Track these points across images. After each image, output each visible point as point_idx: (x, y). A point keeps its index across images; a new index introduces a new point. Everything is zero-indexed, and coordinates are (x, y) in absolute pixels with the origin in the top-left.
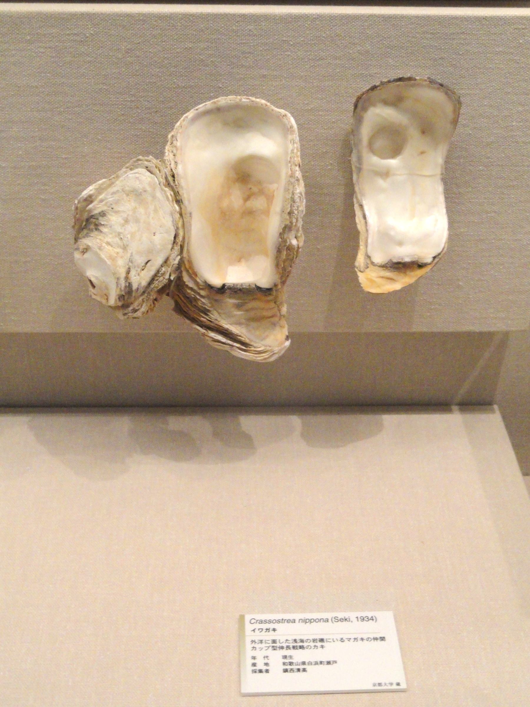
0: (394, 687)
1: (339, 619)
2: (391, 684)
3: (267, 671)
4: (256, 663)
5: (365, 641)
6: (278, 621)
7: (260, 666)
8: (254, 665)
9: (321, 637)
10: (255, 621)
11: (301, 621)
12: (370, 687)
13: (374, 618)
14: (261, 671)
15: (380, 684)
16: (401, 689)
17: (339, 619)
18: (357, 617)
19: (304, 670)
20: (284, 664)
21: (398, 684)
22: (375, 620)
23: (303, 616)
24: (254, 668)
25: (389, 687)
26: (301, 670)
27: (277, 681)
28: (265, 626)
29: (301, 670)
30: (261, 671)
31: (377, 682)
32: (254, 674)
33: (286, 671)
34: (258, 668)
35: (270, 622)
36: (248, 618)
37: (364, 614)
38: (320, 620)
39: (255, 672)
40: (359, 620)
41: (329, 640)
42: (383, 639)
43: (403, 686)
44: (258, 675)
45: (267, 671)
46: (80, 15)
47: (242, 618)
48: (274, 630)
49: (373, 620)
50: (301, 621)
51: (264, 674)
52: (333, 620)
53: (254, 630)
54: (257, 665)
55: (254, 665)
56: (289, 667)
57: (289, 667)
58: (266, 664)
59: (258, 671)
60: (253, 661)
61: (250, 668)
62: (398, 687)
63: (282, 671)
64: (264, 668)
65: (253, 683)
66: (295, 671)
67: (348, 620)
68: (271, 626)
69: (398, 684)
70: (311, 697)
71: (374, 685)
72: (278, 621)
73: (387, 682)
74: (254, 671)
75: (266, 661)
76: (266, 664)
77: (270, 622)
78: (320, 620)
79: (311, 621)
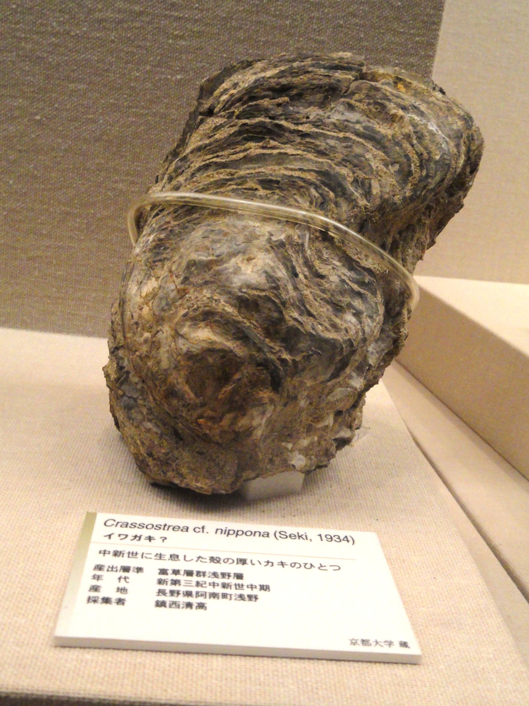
0: (397, 650)
1: (288, 535)
2: (390, 644)
3: (120, 601)
5: (288, 568)
10: (115, 523)
11: (219, 531)
13: (349, 539)
14: (107, 600)
15: (365, 642)
16: (407, 656)
17: (288, 535)
18: (320, 535)
19: (201, 606)
20: (160, 582)
22: (351, 542)
24: (93, 594)
25: (385, 650)
26: (195, 605)
28: (131, 532)
29: (195, 605)
30: (107, 600)
31: (359, 637)
33: (161, 604)
34: (101, 594)
36: (101, 517)
37: (332, 532)
38: (254, 534)
40: (324, 538)
41: (148, 556)
43: (414, 650)
46: (459, 199)
49: (348, 541)
50: (219, 531)
51: (113, 607)
52: (278, 535)
53: (110, 536)
56: (168, 599)
57: (168, 599)
59: (100, 600)
60: (95, 583)
61: (85, 593)
63: (154, 603)
64: (115, 596)
66: (181, 606)
67: (304, 537)
71: (354, 642)
72: (158, 527)
78: (254, 534)
79: (237, 533)
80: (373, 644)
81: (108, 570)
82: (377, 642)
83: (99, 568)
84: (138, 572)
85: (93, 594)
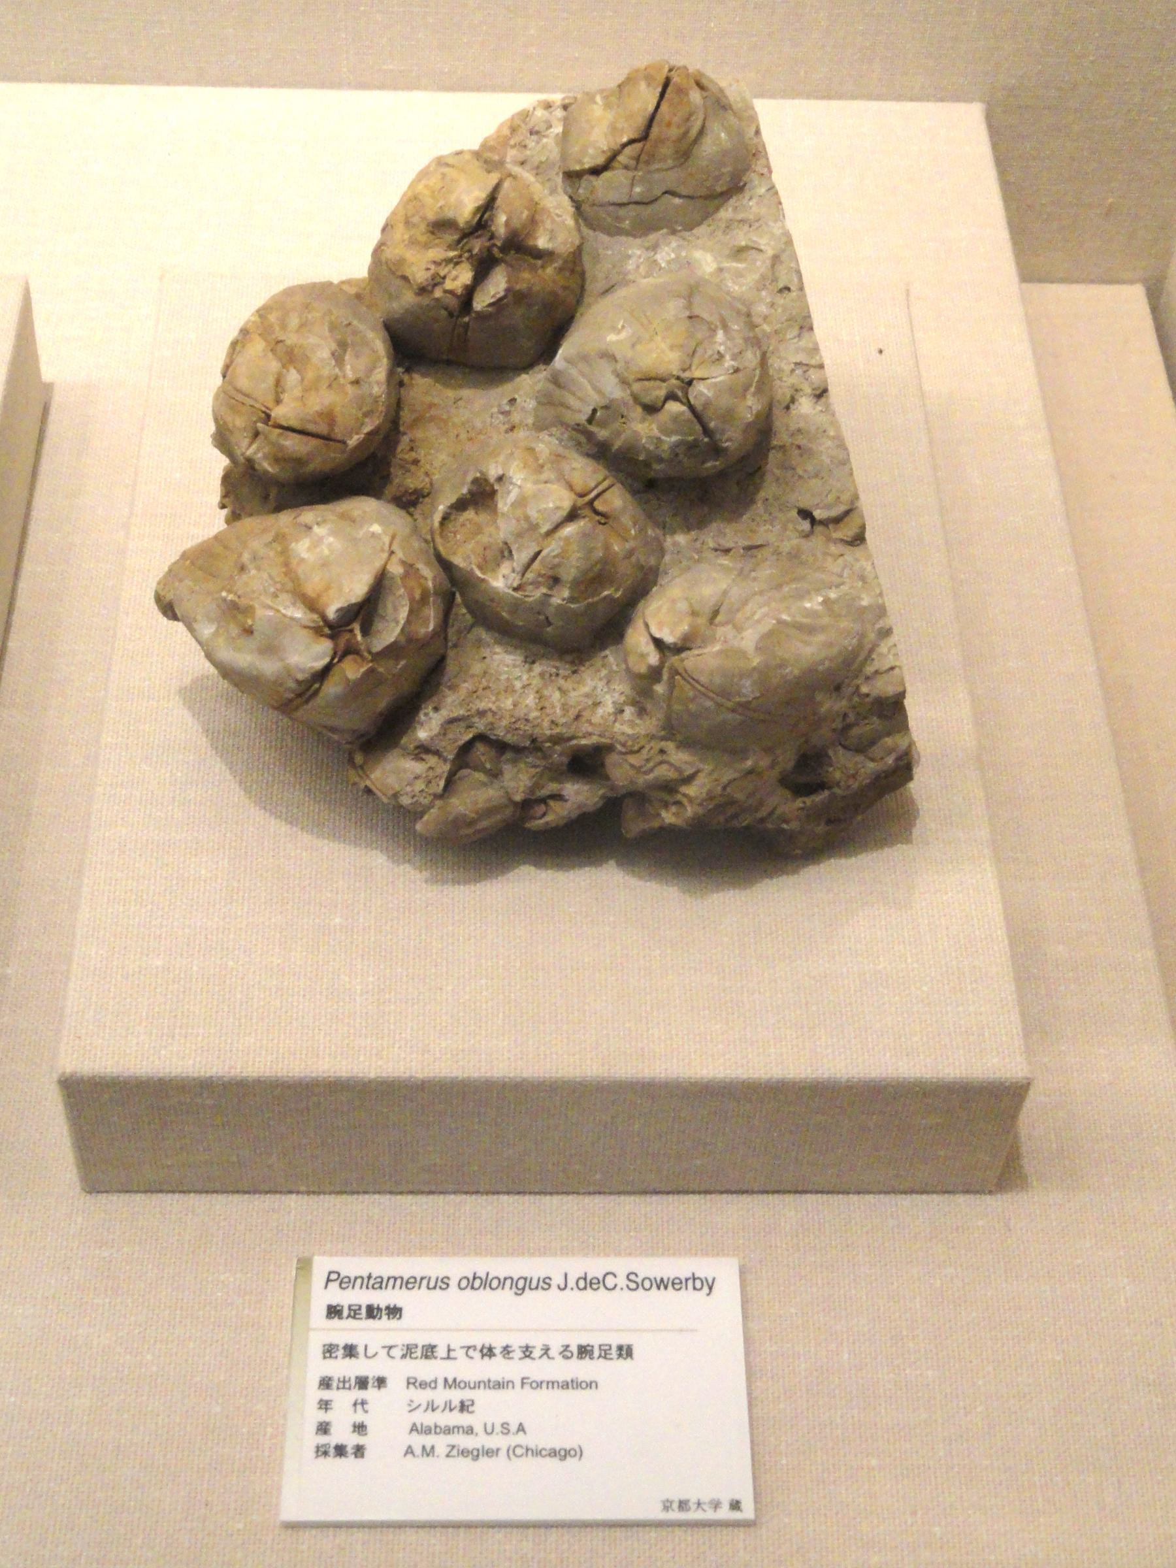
0: (724, 1513)
1: (639, 1280)
2: (716, 1505)
4: (328, 1424)
6: (409, 1283)
7: (341, 1434)
8: (324, 1428)
9: (625, 1340)
12: (656, 1513)
14: (340, 1451)
15: (683, 1505)
21: (735, 1505)
23: (576, 1266)
24: (323, 1440)
25: (709, 1515)
26: (418, 1451)
27: (393, 1483)
30: (340, 1451)
31: (676, 1497)
32: (322, 1459)
33: (409, 1451)
34: (334, 1439)
35: (380, 1283)
36: (322, 1265)
39: (326, 1453)
42: (626, 1352)
43: (748, 1512)
44: (333, 1464)
45: (359, 1451)
47: (305, 1266)
48: (394, 1312)
51: (350, 1461)
54: (333, 1430)
55: (324, 1428)
58: (360, 1428)
59: (332, 1451)
60: (322, 1416)
61: (313, 1439)
62: (736, 1515)
64: (351, 1440)
65: (313, 1489)
68: (382, 1298)
69: (735, 1505)
70: (553, 1535)
73: (705, 1498)
74: (322, 1451)
75: (359, 1417)
76: (360, 1428)
77: (380, 1283)
80: (694, 1507)
81: (338, 1388)
82: (699, 1504)
83: (325, 1383)
84: (379, 1387)
85: (323, 1440)
